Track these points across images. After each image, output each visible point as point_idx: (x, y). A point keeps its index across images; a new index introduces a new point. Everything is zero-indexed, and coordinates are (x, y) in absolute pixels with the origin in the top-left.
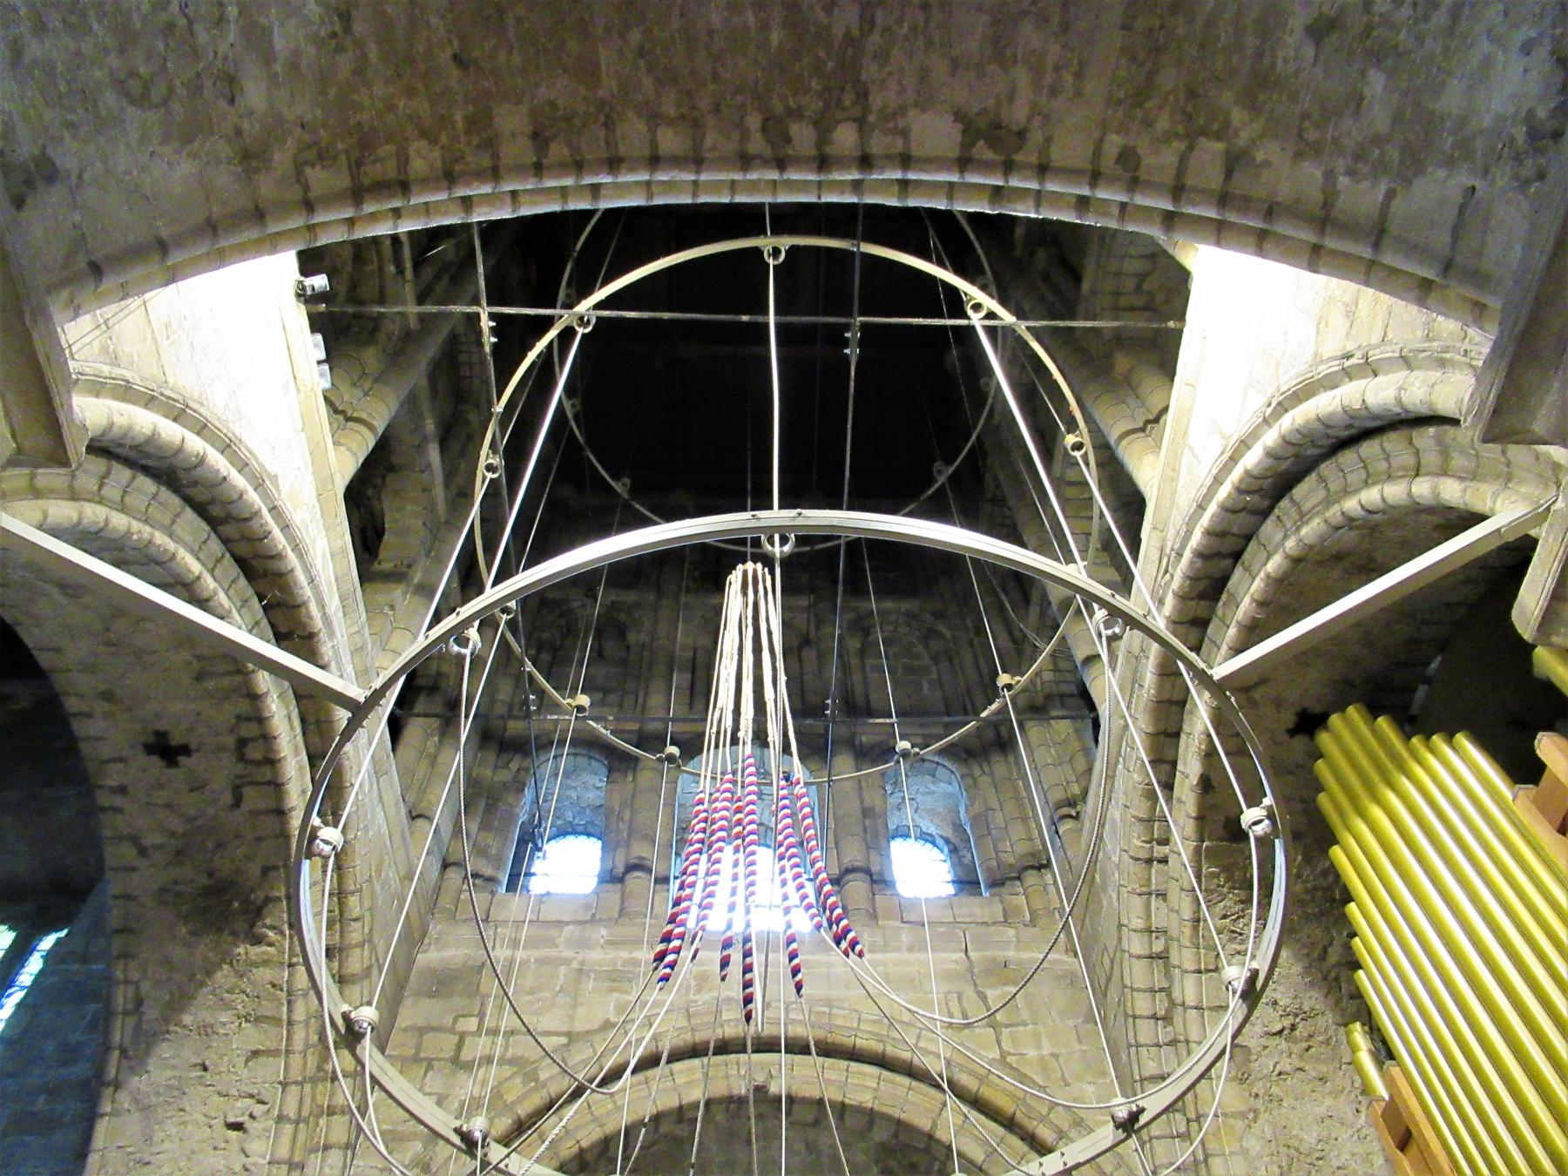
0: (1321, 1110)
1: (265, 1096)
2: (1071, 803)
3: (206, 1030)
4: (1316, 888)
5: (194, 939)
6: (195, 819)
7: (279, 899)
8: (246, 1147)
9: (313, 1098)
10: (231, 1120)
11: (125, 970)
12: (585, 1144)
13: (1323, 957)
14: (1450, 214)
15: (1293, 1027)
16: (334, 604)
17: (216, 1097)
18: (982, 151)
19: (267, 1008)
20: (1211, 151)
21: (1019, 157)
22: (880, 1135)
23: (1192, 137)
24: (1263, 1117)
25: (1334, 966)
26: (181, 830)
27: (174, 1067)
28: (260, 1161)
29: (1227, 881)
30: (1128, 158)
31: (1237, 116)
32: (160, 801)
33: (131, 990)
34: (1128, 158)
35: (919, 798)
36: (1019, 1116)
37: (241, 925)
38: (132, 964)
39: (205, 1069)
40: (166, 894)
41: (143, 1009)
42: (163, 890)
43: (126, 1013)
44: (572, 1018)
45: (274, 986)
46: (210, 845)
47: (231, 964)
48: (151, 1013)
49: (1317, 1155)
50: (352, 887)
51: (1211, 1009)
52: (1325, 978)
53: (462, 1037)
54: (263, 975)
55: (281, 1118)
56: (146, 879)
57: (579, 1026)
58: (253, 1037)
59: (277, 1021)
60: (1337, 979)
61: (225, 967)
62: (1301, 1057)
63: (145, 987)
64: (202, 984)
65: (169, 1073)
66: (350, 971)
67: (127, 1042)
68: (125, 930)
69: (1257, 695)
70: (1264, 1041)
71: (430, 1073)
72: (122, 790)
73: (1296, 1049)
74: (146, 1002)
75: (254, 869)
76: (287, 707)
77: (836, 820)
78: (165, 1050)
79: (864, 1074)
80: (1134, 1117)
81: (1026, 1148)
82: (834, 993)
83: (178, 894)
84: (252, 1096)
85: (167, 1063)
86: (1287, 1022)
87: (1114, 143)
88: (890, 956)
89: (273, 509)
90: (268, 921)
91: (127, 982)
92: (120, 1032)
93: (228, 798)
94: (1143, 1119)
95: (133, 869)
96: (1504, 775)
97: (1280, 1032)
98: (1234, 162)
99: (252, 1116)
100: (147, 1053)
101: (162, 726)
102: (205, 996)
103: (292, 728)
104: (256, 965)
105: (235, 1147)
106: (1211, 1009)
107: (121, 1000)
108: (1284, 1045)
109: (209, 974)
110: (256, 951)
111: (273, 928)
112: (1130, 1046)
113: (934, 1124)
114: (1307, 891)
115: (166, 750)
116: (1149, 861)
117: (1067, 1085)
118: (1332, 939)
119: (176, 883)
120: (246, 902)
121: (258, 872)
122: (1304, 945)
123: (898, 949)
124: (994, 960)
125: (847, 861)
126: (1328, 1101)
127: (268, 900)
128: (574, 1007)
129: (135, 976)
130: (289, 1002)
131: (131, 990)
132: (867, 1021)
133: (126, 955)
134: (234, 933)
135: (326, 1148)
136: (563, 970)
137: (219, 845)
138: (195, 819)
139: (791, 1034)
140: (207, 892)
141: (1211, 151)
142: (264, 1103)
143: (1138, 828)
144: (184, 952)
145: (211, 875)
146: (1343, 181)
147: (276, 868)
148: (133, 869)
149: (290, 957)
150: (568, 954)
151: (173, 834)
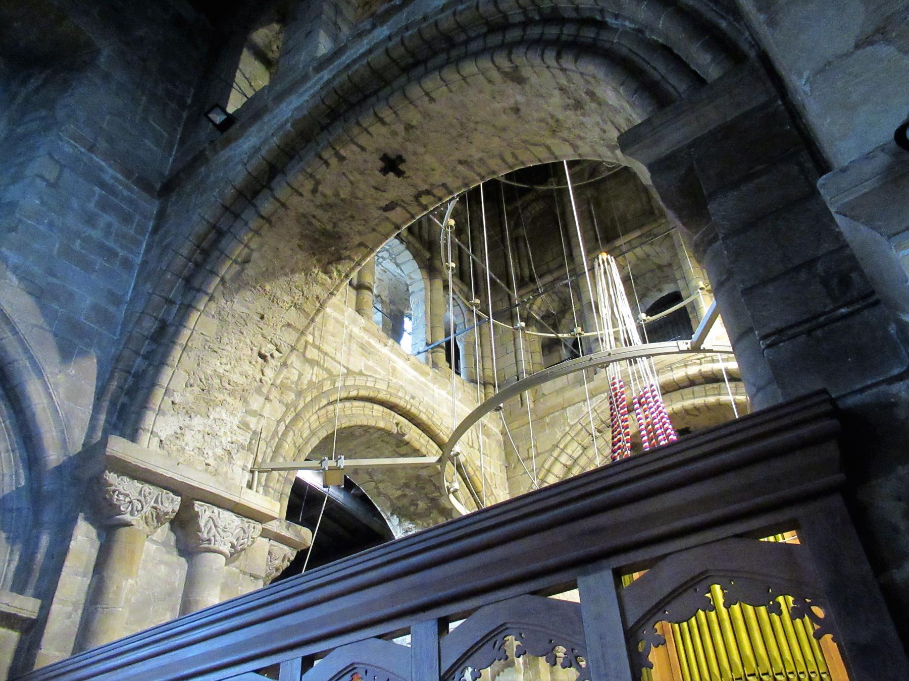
3: (274, 300)
5: (298, 249)
7: (354, 260)
8: (265, 370)
10: (263, 352)
11: (250, 240)
14: (300, 190)
17: (260, 336)
26: (342, 196)
27: (248, 308)
32: (352, 178)
37: (325, 259)
38: (257, 239)
39: (262, 318)
40: (304, 219)
42: (304, 216)
43: (236, 262)
46: (349, 213)
47: (306, 275)
56: (302, 204)
58: (292, 316)
59: (306, 314)
63: (255, 255)
64: (286, 275)
65: (244, 310)
67: (227, 277)
68: (268, 220)
72: (342, 159)
75: (357, 240)
83: (310, 223)
84: (276, 345)
85: (243, 304)
90: (340, 267)
91: (246, 246)
92: (227, 269)
93: (383, 203)
95: (301, 195)
99: (272, 356)
100: (237, 291)
102: (283, 281)
104: (317, 282)
105: (259, 367)
107: (237, 253)
109: (293, 271)
110: (322, 276)
111: (339, 271)
115: (392, 164)
119: (314, 217)
120: (337, 250)
121: (356, 243)
127: (350, 258)
129: (253, 245)
133: (257, 232)
134: (319, 261)
137: (352, 217)
138: (357, 198)
140: (324, 233)
145: (334, 227)
147: (366, 247)
148: (301, 195)
151: (337, 195)
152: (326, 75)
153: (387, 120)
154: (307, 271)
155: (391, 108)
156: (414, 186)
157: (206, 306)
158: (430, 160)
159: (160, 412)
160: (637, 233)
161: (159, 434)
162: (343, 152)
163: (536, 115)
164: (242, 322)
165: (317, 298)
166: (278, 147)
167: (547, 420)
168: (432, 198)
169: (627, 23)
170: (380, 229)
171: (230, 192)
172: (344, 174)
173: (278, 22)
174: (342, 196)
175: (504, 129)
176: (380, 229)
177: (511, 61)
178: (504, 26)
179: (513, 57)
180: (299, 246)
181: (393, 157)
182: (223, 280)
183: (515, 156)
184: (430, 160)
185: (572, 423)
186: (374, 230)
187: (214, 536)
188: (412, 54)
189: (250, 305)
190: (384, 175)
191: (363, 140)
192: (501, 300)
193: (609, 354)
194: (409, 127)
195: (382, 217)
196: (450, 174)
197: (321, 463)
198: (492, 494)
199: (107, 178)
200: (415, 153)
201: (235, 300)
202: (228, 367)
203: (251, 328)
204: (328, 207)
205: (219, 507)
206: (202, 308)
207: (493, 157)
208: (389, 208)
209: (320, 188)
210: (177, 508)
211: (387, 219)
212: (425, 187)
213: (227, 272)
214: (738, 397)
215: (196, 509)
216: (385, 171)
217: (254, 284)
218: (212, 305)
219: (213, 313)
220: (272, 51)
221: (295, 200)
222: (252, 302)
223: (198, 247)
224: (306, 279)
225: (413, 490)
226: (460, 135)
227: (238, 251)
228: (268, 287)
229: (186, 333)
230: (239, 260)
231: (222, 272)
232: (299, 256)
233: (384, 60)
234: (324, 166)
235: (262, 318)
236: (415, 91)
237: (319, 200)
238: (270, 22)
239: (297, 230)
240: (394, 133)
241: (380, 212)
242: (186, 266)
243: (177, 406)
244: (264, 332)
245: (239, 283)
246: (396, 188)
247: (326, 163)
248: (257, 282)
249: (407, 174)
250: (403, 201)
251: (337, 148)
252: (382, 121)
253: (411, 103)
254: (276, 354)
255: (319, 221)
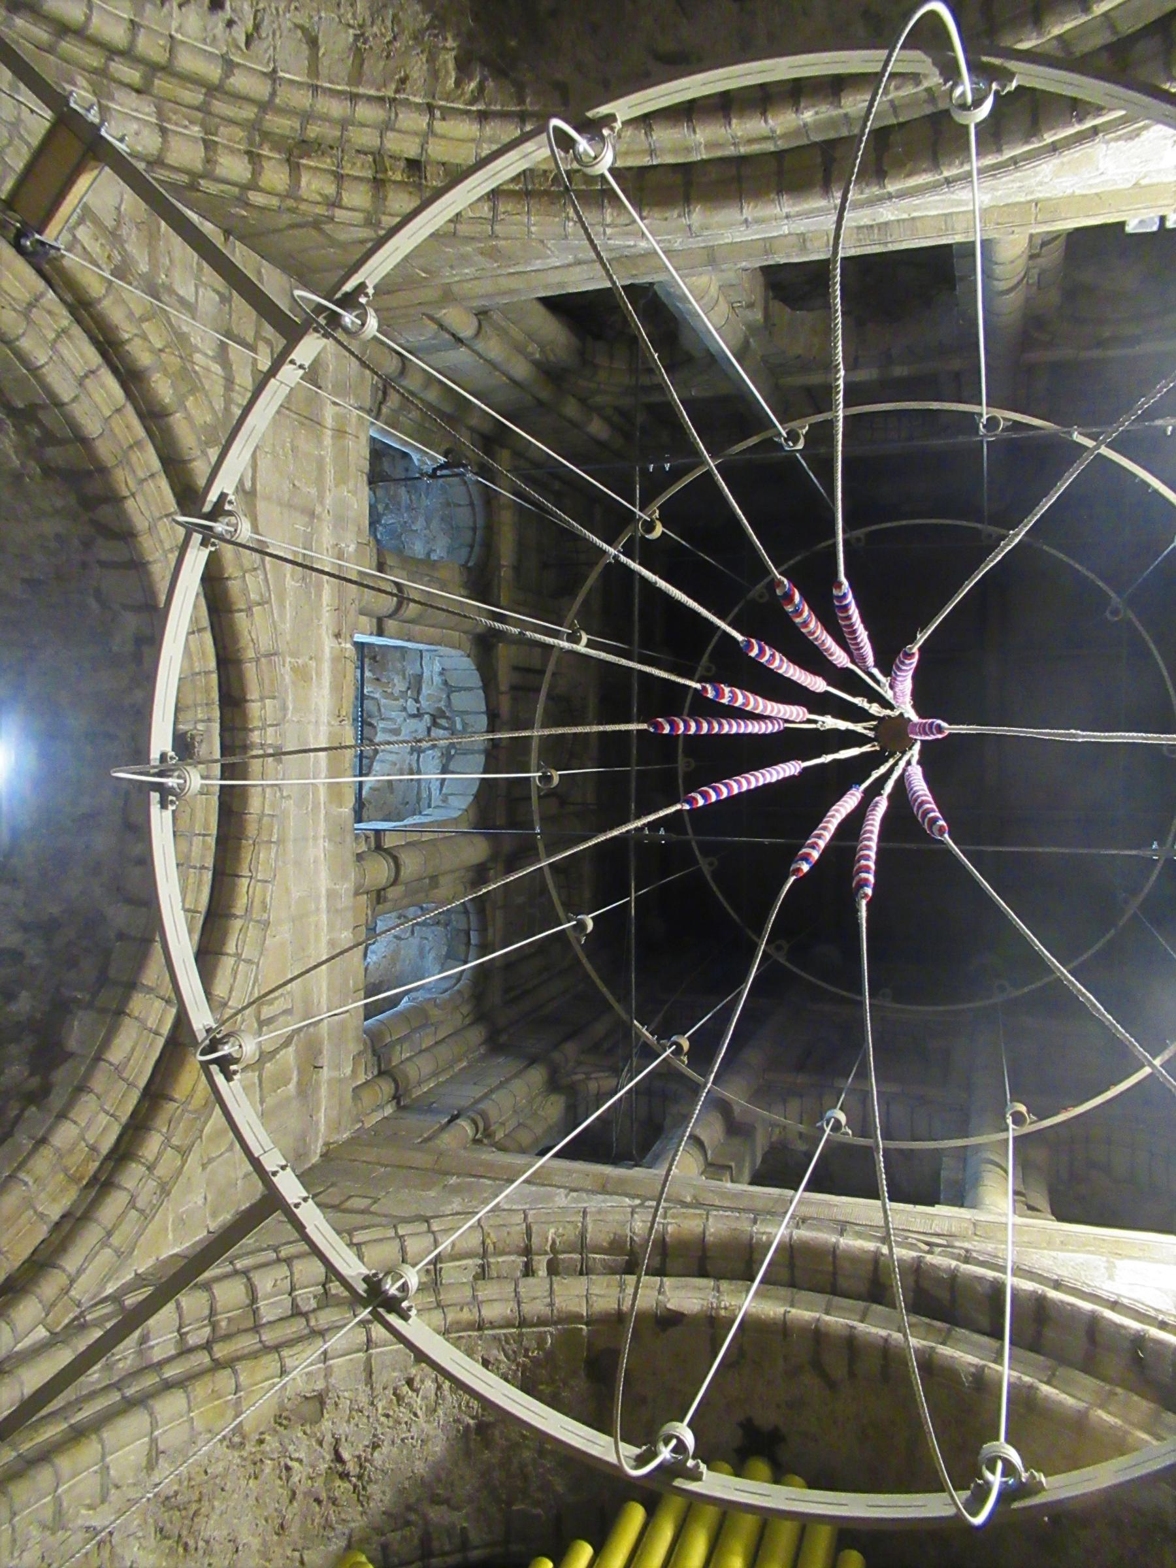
0: (245, 1537)
1: (259, 47)
2: (488, 1134)
4: (525, 1478)
7: (521, 101)
9: (232, 122)
12: (130, 504)
13: (435, 1500)
15: (345, 1476)
16: (887, 213)
19: (374, 67)
22: (119, 916)
24: (234, 1456)
25: (424, 1516)
28: (174, 25)
29: (533, 1359)
35: (415, 941)
44: (268, 498)
45: (403, 81)
47: (430, 26)
49: (191, 1543)
50: (501, 209)
51: (369, 1359)
52: (409, 1508)
53: (253, 348)
54: (417, 68)
55: (229, 66)
57: (261, 505)
59: (357, 77)
60: (408, 1523)
61: (428, 18)
62: (307, 1494)
66: (391, 195)
69: (809, 1379)
70: (329, 1439)
71: (217, 298)
73: (319, 1483)
76: (784, 136)
77: (432, 842)
79: (199, 890)
80: (393, 1305)
81: (124, 1119)
82: (290, 846)
84: (257, 27)
86: (352, 1467)
88: (324, 917)
89: (1095, 131)
90: (490, 84)
94: (392, 1318)
97: (338, 1458)
99: (230, 24)
103: (750, 141)
104: (431, 59)
106: (369, 1359)
108: (323, 1467)
111: (481, 88)
112: (276, 1249)
113: (150, 990)
114: (522, 1466)
116: (527, 1251)
117: (204, 1166)
118: (457, 1508)
121: (559, 76)
122: (449, 1473)
123: (331, 927)
124: (321, 1052)
125: (406, 859)
126: (256, 1543)
128: (280, 504)
130: (381, 99)
132: (264, 891)
135: (164, 131)
136: (313, 491)
139: (253, 790)
142: (248, 44)
143: (571, 1234)
149: (440, 107)
150: (328, 501)
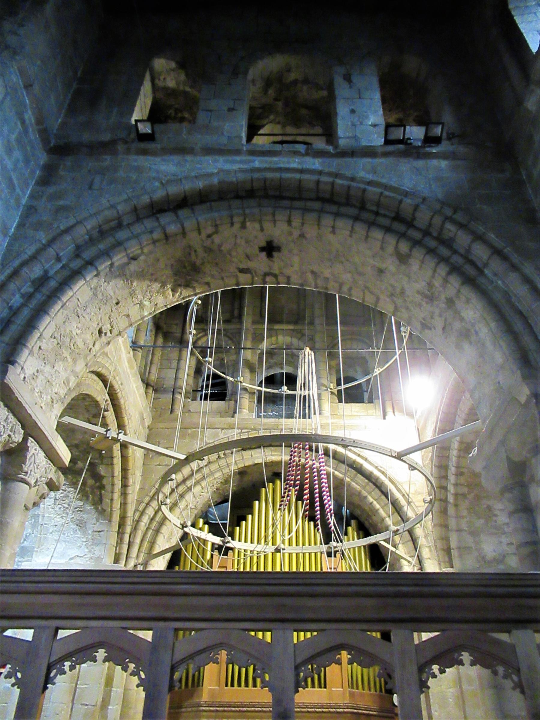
6: (230, 255)
18: (464, 446)
20: (465, 490)
21: (462, 452)
23: (468, 486)
26: (222, 248)
27: (115, 292)
30: (462, 474)
31: (472, 495)
33: (139, 251)
34: (462, 474)
36: (130, 488)
38: (151, 247)
39: (117, 304)
40: (189, 250)
41: (133, 262)
48: (133, 267)
56: (194, 239)
63: (142, 258)
65: (112, 294)
67: (116, 264)
74: (136, 262)
75: (208, 279)
78: (120, 282)
84: (112, 327)
87: (465, 470)
91: (142, 248)
92: (119, 259)
93: (242, 266)
95: (200, 233)
96: (254, 507)
98: (464, 495)
99: (106, 334)
101: (285, 251)
107: (133, 250)
109: (156, 280)
111: (181, 293)
115: (270, 249)
119: (195, 251)
127: (194, 288)
129: (146, 250)
131: (139, 251)
134: (176, 281)
138: (230, 255)
141: (465, 490)
144: (163, 266)
146: (465, 520)
147: (209, 286)
148: (200, 233)
152: (258, 162)
153: (294, 224)
154: (163, 285)
155: (303, 219)
156: (270, 267)
157: (91, 279)
158: (296, 260)
159: (31, 353)
160: (291, 327)
161: (26, 371)
162: (248, 224)
163: (392, 282)
164: (105, 301)
165: (156, 305)
166: (200, 190)
167: (189, 431)
168: (274, 280)
169: (499, 282)
170: (226, 280)
171: (145, 199)
172: (236, 236)
173: (177, 63)
174: (222, 248)
175: (360, 274)
176: (226, 280)
177: (410, 251)
178: (410, 224)
179: (414, 250)
180: (172, 265)
181: (275, 245)
182: (112, 265)
183: (350, 289)
184: (296, 260)
185: (208, 441)
186: (223, 279)
187: (31, 471)
188: (332, 194)
189: (117, 291)
190: (260, 251)
191: (267, 225)
192: (177, 325)
193: (343, 440)
194: (302, 236)
195: (235, 274)
196: (299, 274)
197: (107, 431)
198: (135, 474)
199: (27, 117)
200: (290, 251)
201: (111, 283)
202: (79, 332)
203: (106, 309)
204: (208, 250)
205: (40, 447)
206: (88, 279)
207: (335, 282)
208: (242, 271)
209: (215, 237)
210: (20, 441)
211: (237, 276)
212: (277, 272)
213: (118, 260)
214: (337, 473)
215: (29, 445)
216: (262, 249)
217: (128, 277)
218: (95, 280)
219: (92, 286)
220: (159, 79)
221: (195, 234)
222: (119, 290)
223: (100, 226)
224: (159, 290)
225: (80, 452)
226: (330, 260)
227: (134, 249)
228: (135, 284)
229: (70, 293)
230: (131, 255)
231: (115, 259)
232: (167, 272)
233: (312, 186)
234: (229, 225)
235: (117, 304)
236: (327, 220)
237: (208, 243)
238: (173, 59)
239: (179, 254)
240: (291, 234)
241: (236, 270)
242: (83, 236)
243: (41, 351)
244: (112, 314)
245: (121, 272)
246: (261, 263)
247: (232, 224)
248: (131, 276)
249: (274, 259)
250: (255, 272)
251: (247, 220)
252: (289, 222)
253: (318, 225)
254: (109, 334)
255: (197, 256)
